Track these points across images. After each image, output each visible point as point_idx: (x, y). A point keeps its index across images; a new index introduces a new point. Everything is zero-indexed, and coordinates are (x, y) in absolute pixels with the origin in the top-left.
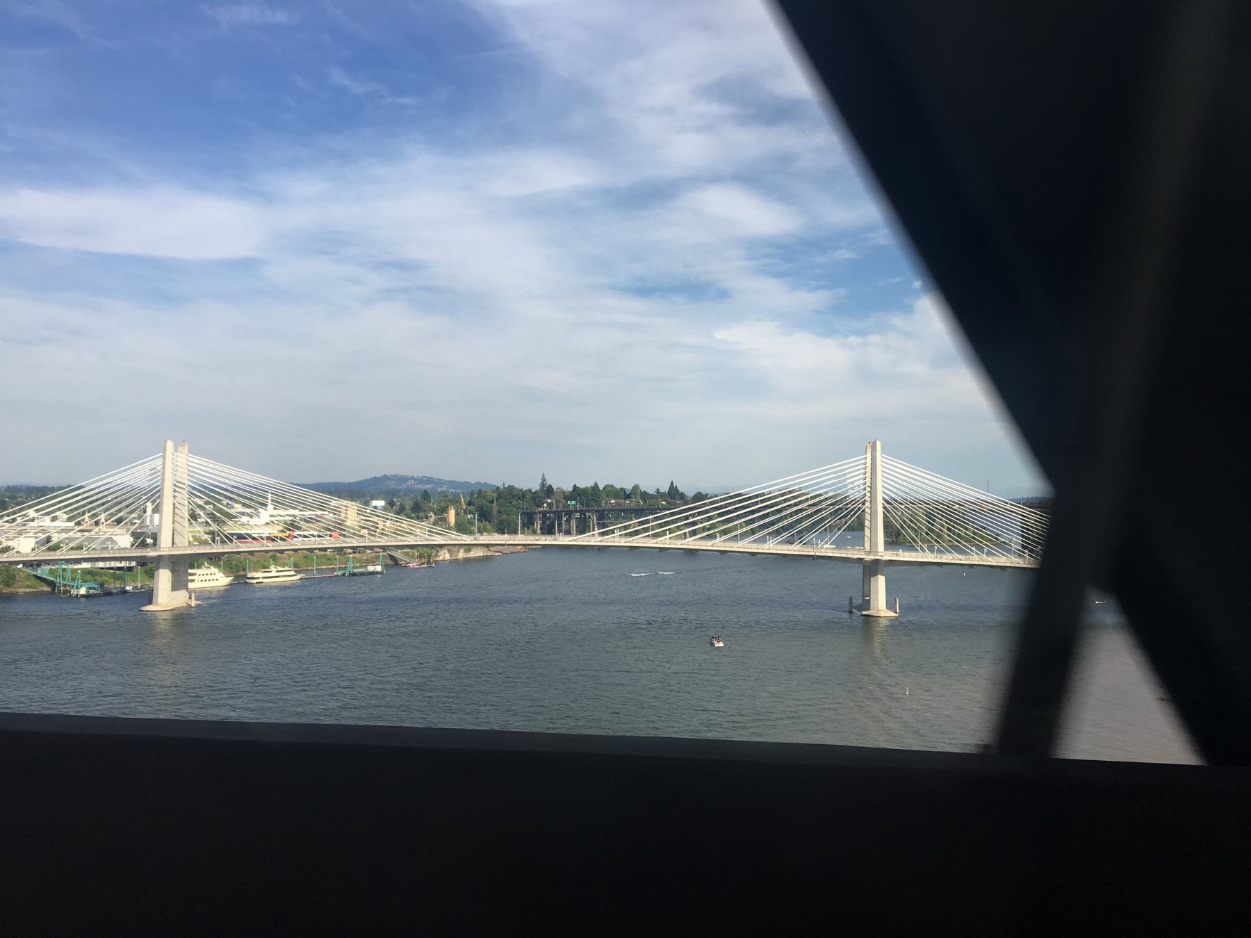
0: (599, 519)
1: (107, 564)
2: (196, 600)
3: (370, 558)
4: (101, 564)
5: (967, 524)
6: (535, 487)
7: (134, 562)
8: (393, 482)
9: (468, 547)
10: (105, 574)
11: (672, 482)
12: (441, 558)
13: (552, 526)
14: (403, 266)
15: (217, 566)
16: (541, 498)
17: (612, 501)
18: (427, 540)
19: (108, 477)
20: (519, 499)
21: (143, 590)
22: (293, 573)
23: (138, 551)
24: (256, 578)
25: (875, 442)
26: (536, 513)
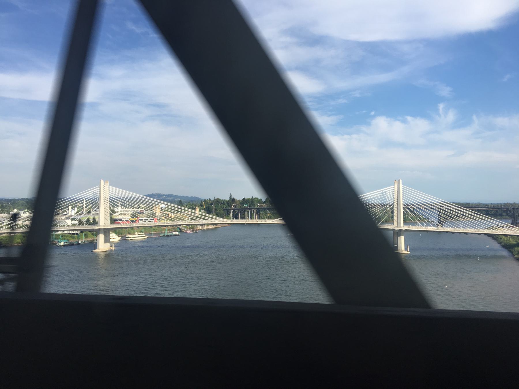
0: (257, 212)
1: (68, 232)
2: (114, 247)
3: (170, 228)
4: (66, 232)
5: (153, 205)
6: (227, 198)
7: (79, 231)
8: (156, 196)
9: (208, 225)
10: (68, 236)
11: (231, 193)
12: (198, 229)
13: (237, 214)
14: (159, 106)
15: (115, 233)
16: (231, 203)
17: (259, 205)
18: (211, 222)
19: (80, 194)
20: (222, 203)
21: (86, 243)
22: (144, 235)
23: (89, 227)
24: (130, 238)
25: (399, 180)
26: (230, 210)
